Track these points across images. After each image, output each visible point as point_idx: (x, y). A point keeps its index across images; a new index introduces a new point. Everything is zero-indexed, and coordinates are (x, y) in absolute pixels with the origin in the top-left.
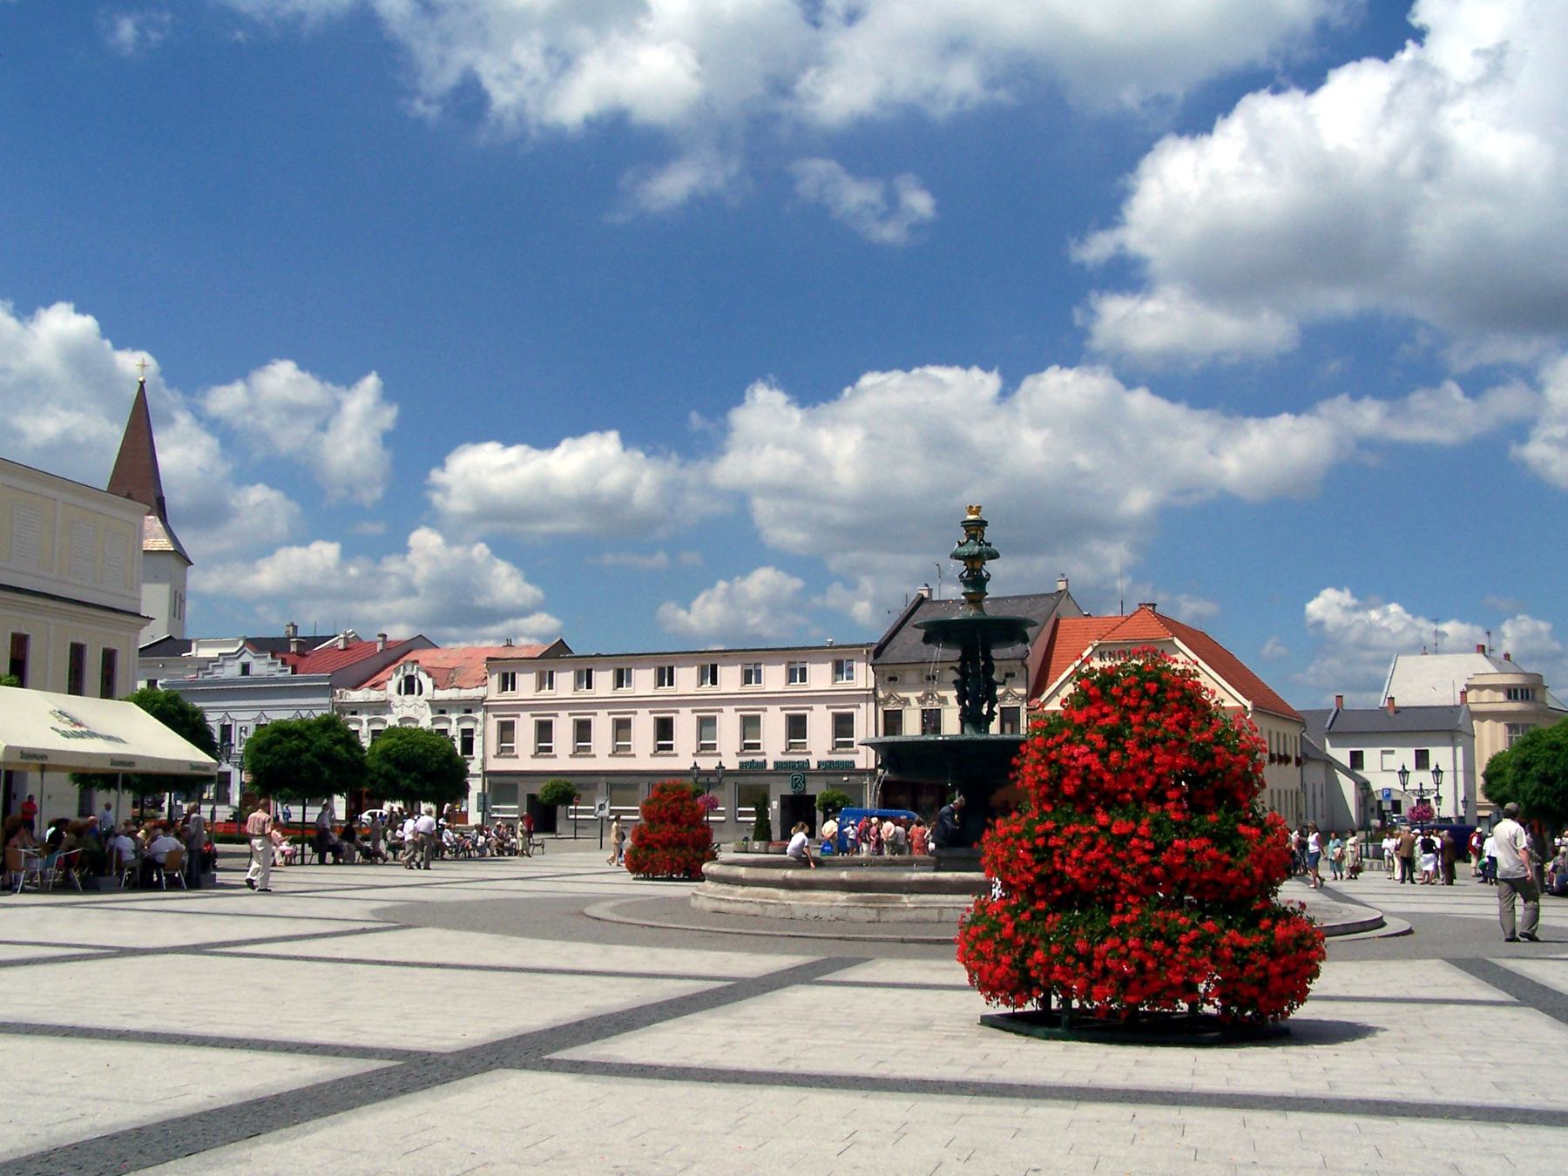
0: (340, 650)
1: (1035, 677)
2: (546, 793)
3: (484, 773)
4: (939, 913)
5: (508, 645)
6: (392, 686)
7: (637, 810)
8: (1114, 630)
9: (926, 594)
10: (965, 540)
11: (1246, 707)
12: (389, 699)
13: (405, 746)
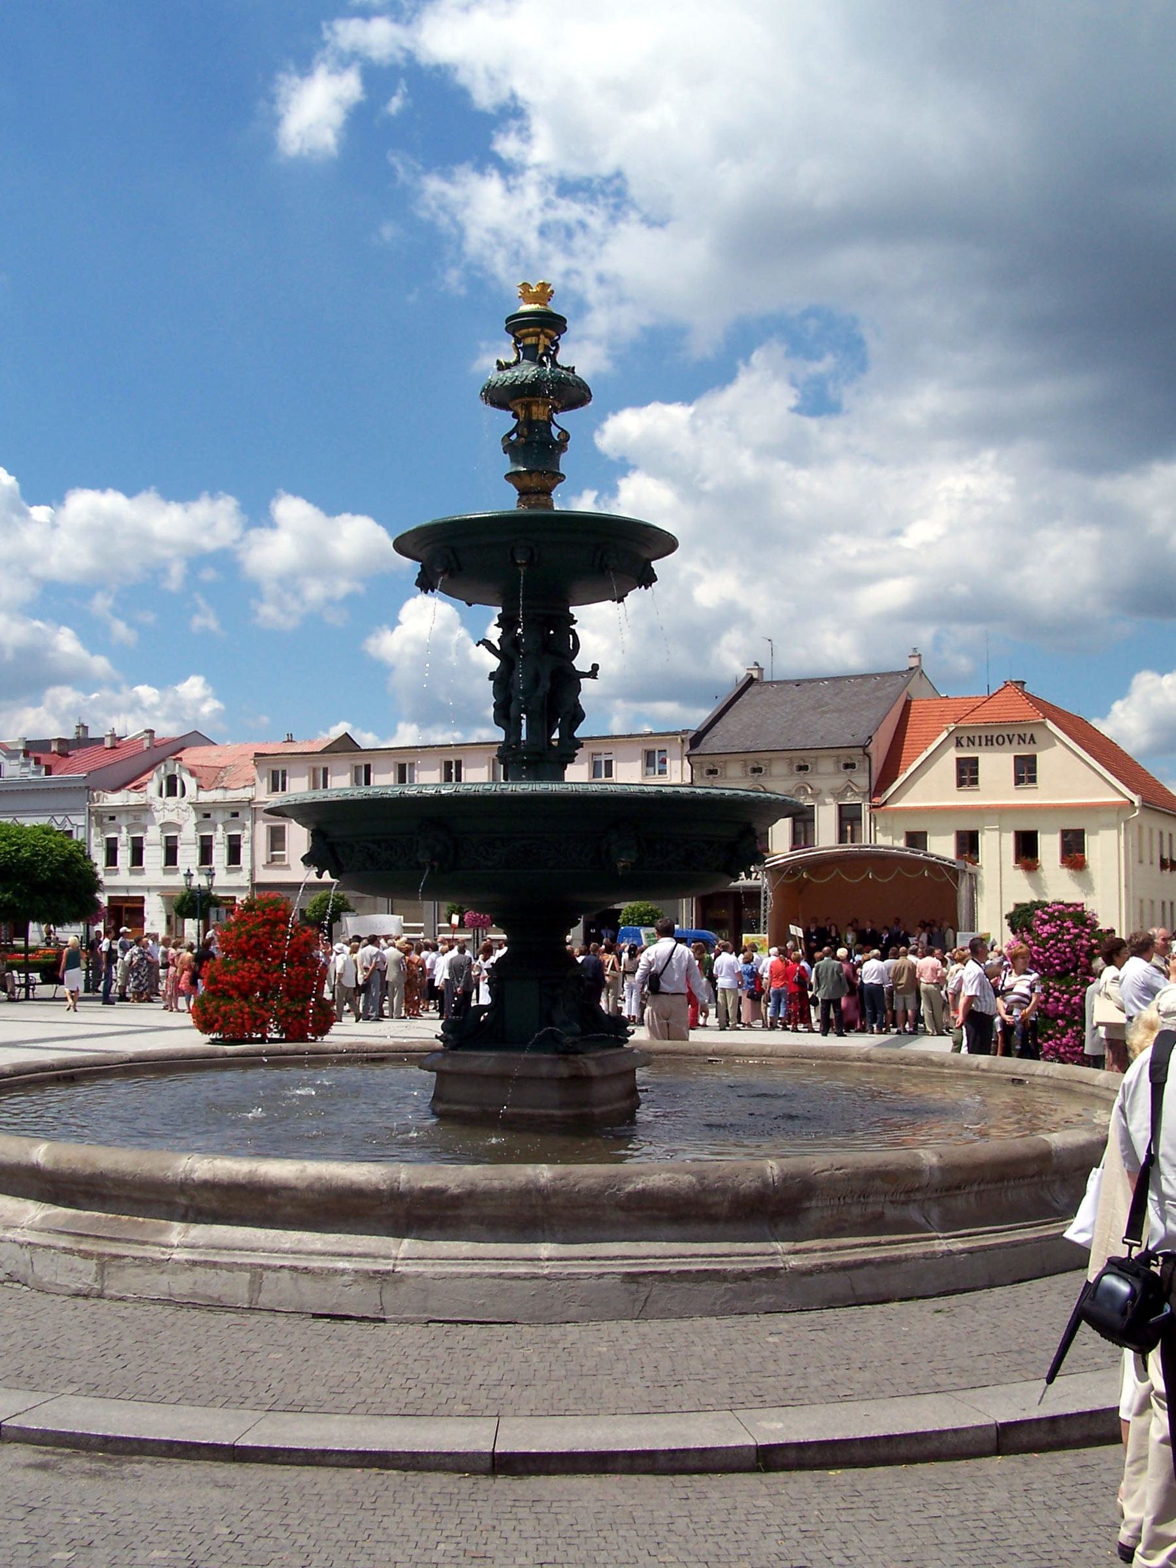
0: (107, 749)
1: (880, 765)
2: (315, 907)
3: (253, 885)
4: (252, 1282)
5: (288, 741)
6: (152, 788)
7: (422, 928)
8: (973, 711)
9: (755, 675)
10: (513, 359)
11: (1132, 802)
12: (150, 802)
13: (8, 849)
